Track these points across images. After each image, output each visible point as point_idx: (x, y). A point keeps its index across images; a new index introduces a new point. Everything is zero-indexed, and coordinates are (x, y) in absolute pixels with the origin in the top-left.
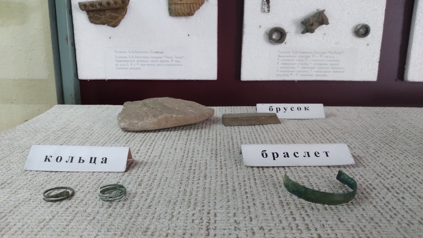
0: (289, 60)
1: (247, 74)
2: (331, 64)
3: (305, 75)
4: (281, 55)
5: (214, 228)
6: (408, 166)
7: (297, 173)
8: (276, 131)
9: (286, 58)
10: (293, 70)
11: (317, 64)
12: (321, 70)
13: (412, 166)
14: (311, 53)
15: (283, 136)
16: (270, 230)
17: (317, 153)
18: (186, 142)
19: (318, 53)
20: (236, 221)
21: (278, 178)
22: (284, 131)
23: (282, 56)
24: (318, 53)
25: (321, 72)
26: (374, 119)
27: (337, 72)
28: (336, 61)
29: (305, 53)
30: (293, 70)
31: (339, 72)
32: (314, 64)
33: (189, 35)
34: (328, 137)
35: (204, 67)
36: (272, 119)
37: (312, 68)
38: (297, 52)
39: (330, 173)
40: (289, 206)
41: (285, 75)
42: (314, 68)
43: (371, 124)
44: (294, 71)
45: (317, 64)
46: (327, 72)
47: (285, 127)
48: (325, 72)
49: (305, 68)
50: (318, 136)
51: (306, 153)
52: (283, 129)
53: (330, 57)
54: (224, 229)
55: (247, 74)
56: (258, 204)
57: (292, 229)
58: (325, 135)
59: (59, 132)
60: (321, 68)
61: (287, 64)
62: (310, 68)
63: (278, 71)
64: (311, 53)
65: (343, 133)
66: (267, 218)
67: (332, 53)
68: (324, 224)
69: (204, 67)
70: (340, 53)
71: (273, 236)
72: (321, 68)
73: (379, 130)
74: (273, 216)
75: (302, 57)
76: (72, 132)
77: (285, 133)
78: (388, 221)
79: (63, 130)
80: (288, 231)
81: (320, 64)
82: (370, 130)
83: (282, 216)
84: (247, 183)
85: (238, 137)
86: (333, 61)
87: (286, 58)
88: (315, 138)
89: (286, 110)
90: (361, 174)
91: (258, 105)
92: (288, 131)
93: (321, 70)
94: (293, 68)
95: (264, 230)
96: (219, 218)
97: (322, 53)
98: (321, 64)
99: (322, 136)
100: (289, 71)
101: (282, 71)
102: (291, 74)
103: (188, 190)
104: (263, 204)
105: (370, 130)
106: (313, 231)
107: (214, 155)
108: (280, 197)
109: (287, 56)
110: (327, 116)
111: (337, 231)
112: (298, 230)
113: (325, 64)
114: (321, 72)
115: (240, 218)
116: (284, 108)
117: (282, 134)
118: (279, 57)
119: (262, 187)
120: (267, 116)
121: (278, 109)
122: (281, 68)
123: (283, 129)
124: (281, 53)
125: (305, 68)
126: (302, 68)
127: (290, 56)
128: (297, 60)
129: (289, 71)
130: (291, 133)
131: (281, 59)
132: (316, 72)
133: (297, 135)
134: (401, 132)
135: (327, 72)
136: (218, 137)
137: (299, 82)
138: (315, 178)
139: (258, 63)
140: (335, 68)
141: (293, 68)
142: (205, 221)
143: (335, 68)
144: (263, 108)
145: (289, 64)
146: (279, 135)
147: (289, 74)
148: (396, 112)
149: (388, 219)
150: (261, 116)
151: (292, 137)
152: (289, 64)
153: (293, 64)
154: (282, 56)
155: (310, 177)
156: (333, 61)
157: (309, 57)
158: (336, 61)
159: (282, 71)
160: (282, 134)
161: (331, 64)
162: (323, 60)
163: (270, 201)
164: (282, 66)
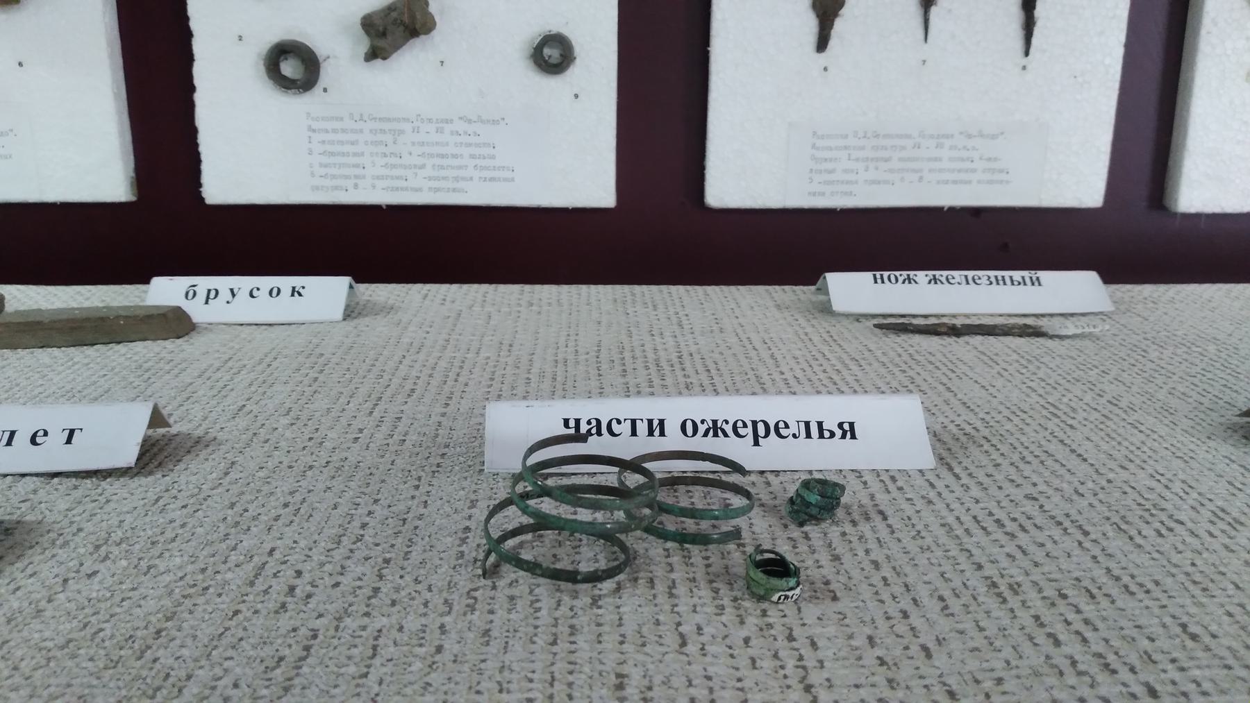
0: (341, 143)
1: (219, 186)
2: (472, 157)
3: (397, 189)
4: (315, 125)
5: (826, 683)
7: (1000, 488)
9: (331, 137)
10: (359, 171)
11: (431, 156)
12: (443, 173)
14: (406, 120)
16: (999, 681)
17: (781, 425)
19: (430, 120)
21: (948, 506)
23: (320, 131)
24: (932, 137)
25: (444, 178)
27: (492, 179)
28: (486, 145)
29: (389, 120)
30: (359, 171)
31: (499, 179)
32: (422, 155)
33: (20, 64)
34: (1041, 374)
35: (1076, 175)
36: (175, 324)
37: (415, 166)
38: (365, 118)
40: (1020, 598)
41: (336, 188)
42: (423, 167)
43: (1148, 336)
44: (364, 177)
45: (431, 156)
46: (464, 179)
48: (456, 179)
49: (394, 166)
51: (802, 426)
53: (965, 147)
54: (857, 686)
55: (219, 186)
57: (1061, 674)
59: (219, 375)
60: (442, 167)
61: (339, 154)
62: (410, 167)
63: (313, 175)
64: (406, 120)
66: (971, 644)
67: (470, 121)
68: (1149, 650)
71: (1015, 698)
72: (442, 167)
73: (1179, 351)
74: (987, 633)
75: (383, 131)
76: (260, 368)
77: (912, 363)
79: (230, 364)
80: (1052, 680)
81: (438, 155)
83: (1015, 632)
86: (478, 145)
87: (331, 137)
89: (234, 295)
91: (156, 281)
92: (917, 357)
93: (443, 173)
94: (356, 166)
96: (830, 653)
97: (442, 121)
98: (443, 156)
100: (347, 177)
101: (325, 176)
102: (356, 186)
104: (941, 599)
105: (1154, 355)
108: (980, 567)
109: (335, 131)
110: (351, 312)
111: (1197, 672)
112: (1080, 674)
113: (455, 156)
114: (444, 178)
115: (890, 647)
116: (232, 290)
117: (904, 367)
118: (310, 134)
119: (914, 538)
120: (135, 317)
121: (213, 294)
122: (321, 165)
123: (900, 350)
124: (317, 119)
125: (394, 166)
126: (386, 166)
127: (344, 131)
128: (366, 143)
129: (347, 177)
130: (931, 363)
131: (317, 137)
132: (430, 179)
135: (464, 179)
137: (393, 209)
138: (1056, 498)
140: (487, 168)
141: (356, 166)
142: (791, 663)
143: (487, 168)
144: (166, 291)
145: (343, 154)
146: (896, 370)
147: (349, 184)
150: (118, 317)
151: (938, 374)
152: (343, 154)
153: (355, 154)
154: (320, 131)
155: (1042, 500)
156: (478, 145)
157: (402, 132)
158: (486, 145)
159: (325, 176)
160: (904, 367)
161: (472, 157)
162: (447, 144)
163: (957, 583)
164: (325, 160)
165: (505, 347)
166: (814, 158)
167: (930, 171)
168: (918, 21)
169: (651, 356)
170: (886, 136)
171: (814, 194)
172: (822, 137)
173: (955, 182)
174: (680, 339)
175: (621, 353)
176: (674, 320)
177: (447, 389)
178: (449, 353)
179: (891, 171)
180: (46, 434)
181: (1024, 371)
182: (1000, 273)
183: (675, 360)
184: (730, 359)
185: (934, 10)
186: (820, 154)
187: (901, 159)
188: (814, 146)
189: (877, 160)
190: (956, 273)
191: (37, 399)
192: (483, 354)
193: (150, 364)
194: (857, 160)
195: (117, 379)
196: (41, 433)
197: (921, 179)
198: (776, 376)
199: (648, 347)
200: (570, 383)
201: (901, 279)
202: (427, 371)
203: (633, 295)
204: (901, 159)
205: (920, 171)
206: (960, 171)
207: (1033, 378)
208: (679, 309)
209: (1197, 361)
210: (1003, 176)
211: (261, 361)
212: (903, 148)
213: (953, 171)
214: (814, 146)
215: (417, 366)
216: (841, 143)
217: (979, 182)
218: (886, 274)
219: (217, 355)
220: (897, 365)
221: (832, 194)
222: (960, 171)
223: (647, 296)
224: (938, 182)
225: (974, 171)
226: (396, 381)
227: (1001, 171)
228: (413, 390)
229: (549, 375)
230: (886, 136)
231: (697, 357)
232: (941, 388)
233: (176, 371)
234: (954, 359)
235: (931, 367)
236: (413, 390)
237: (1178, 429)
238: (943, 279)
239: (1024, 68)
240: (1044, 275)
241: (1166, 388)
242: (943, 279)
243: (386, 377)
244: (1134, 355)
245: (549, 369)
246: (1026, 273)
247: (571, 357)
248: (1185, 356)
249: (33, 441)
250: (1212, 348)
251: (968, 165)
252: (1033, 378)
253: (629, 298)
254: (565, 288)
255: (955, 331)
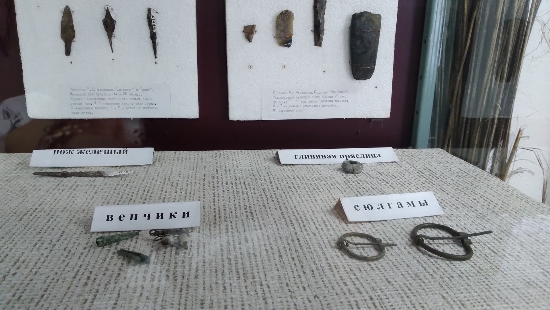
4: (276, 96)
6: (446, 218)
8: (309, 179)
13: (450, 218)
15: (318, 185)
18: (214, 199)
20: (290, 291)
22: (317, 178)
24: (121, 90)
26: (410, 162)
34: (364, 186)
35: (183, 102)
39: (372, 228)
43: (407, 169)
47: (318, 174)
50: (353, 184)
51: (380, 205)
52: (316, 176)
56: (307, 272)
58: (361, 184)
65: (380, 182)
69: (183, 102)
70: (147, 90)
77: (319, 181)
78: (431, 275)
82: (406, 177)
84: (292, 245)
85: (270, 187)
88: (351, 186)
90: (402, 226)
91: (35, 152)
95: (318, 298)
99: (358, 185)
103: (232, 257)
106: (364, 293)
107: (249, 214)
117: (316, 182)
123: (316, 176)
130: (325, 181)
133: (332, 183)
134: (438, 176)
136: (248, 190)
139: (245, 104)
148: (431, 153)
149: (431, 273)
160: (316, 182)
165: (167, 177)
166: (72, 98)
167: (122, 104)
168: (108, 43)
169: (224, 179)
170: (101, 90)
171: (75, 113)
172: (74, 90)
173: (134, 108)
174: (236, 172)
175: (213, 179)
176: (235, 164)
177: (144, 196)
178: (145, 181)
179: (106, 104)
180: (124, 216)
181: (358, 185)
182: (110, 149)
183: (234, 182)
184: (254, 181)
185: (113, 40)
186: (74, 97)
187: (109, 99)
188: (71, 94)
189: (99, 99)
190: (91, 150)
191: (131, 201)
192: (159, 181)
193: (26, 188)
194: (91, 99)
195: (13, 195)
196: (122, 216)
197: (119, 107)
198: (270, 187)
199: (224, 176)
200: (192, 193)
201: (66, 152)
202: (137, 190)
203: (220, 154)
204: (109, 99)
205: (119, 104)
206: (135, 104)
207: (361, 187)
208: (237, 160)
209: (421, 179)
210: (154, 106)
211: (71, 188)
212: (109, 95)
213: (131, 104)
214: (71, 94)
215: (133, 188)
216: (83, 92)
217: (144, 108)
218: (60, 150)
219: (53, 183)
220: (314, 181)
221: (82, 113)
222: (135, 104)
223: (226, 154)
224: (127, 108)
225: (142, 104)
226: (125, 195)
227: (153, 104)
228: (131, 199)
229: (184, 190)
230: (101, 90)
231: (242, 180)
232: (327, 191)
233: (37, 190)
234: (334, 180)
235: (325, 183)
236: (131, 199)
237: (531, 203)
238: (85, 152)
239: (156, 63)
240: (129, 150)
241: (408, 188)
242: (85, 152)
243: (121, 194)
244: (400, 175)
245: (184, 187)
246: (122, 149)
247: (193, 182)
248: (418, 177)
249: (120, 219)
250: (427, 174)
251: (138, 101)
252: (361, 187)
253: (218, 155)
254: (193, 152)
255: (65, 175)
